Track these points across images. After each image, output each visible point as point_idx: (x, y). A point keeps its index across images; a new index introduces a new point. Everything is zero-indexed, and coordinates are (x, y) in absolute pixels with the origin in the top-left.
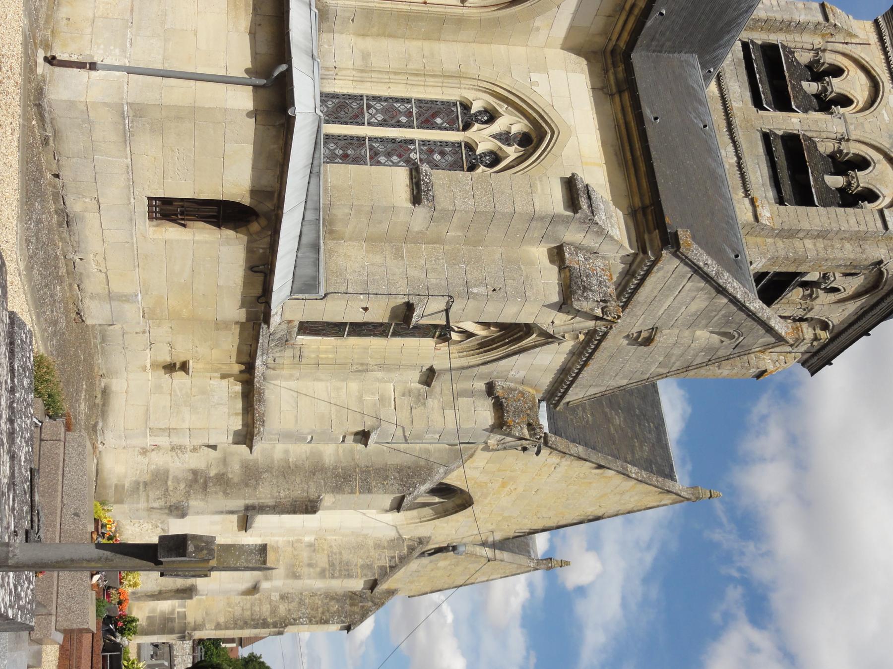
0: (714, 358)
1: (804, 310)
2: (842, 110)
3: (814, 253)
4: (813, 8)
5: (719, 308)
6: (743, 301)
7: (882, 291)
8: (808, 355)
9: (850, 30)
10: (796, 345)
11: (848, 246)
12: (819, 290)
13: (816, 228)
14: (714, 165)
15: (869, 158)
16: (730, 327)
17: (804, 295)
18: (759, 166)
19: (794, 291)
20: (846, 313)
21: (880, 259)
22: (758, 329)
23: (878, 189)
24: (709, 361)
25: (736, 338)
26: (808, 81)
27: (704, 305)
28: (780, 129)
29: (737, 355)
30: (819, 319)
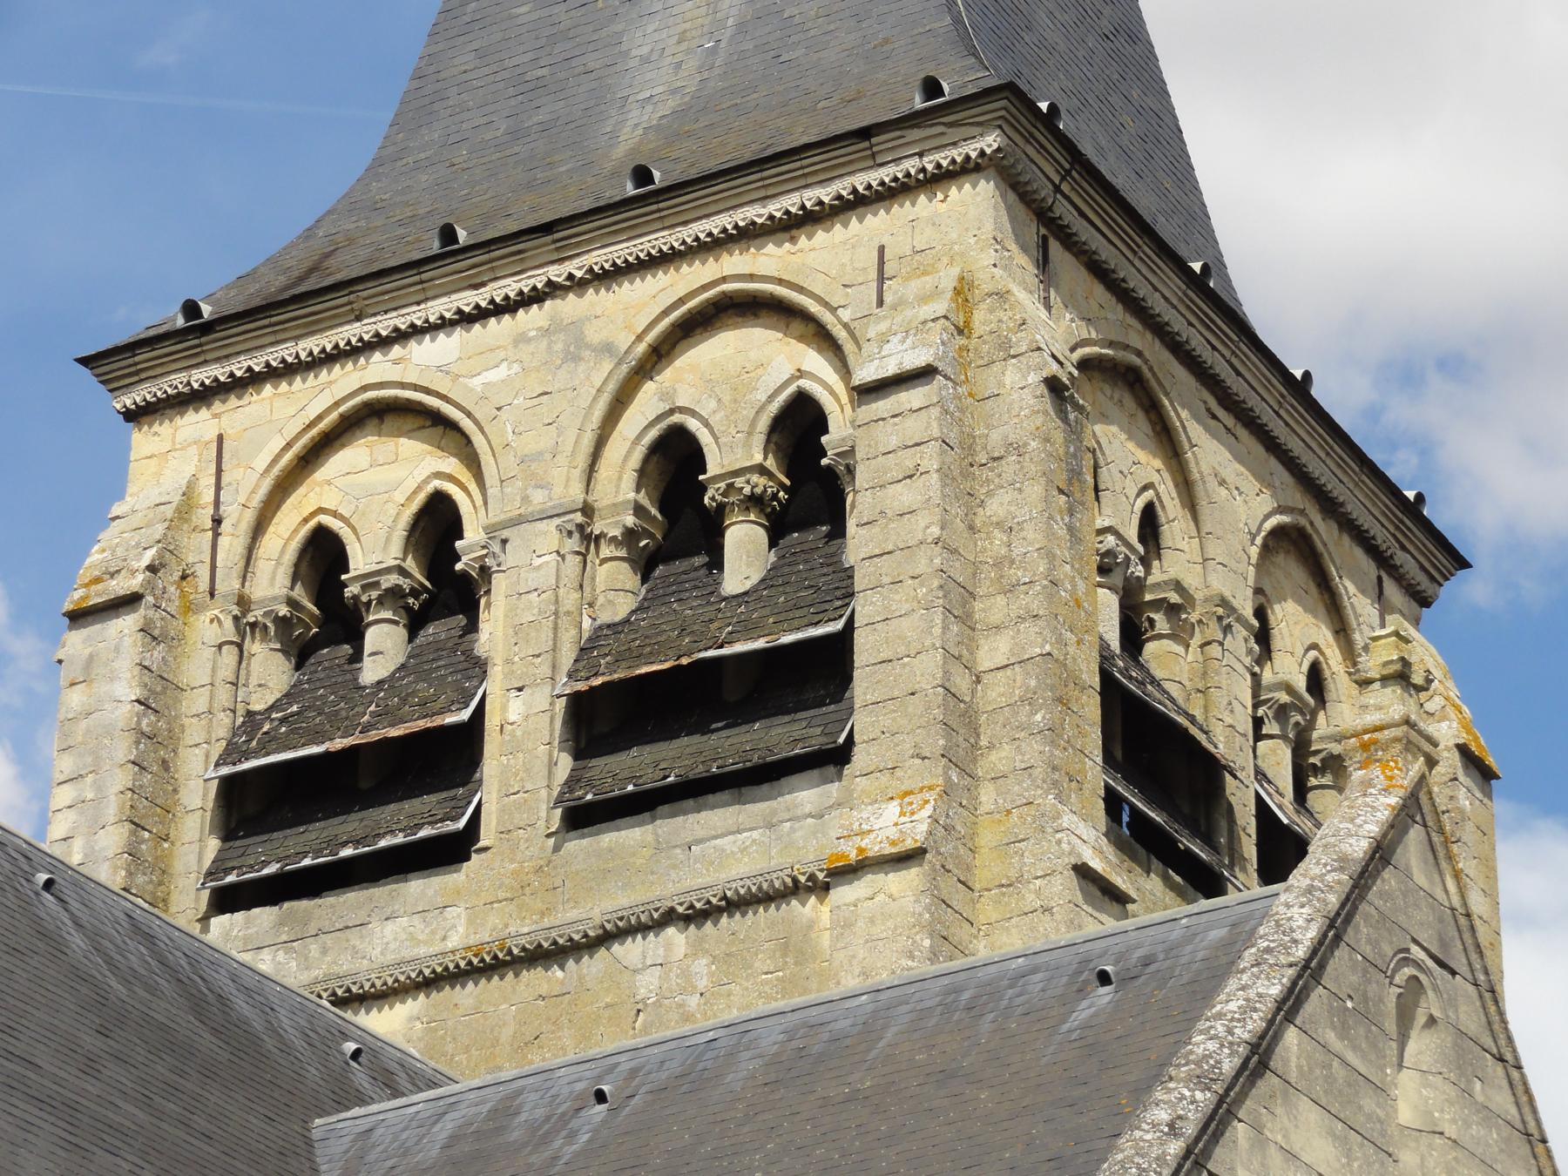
0: (1488, 1042)
1: (1227, 629)
2: (472, 535)
3: (1030, 629)
4: (88, 651)
5: (1319, 1056)
6: (1291, 972)
7: (1147, 354)
8: (1390, 587)
9: (169, 511)
10: (1427, 747)
11: (997, 506)
12: (1150, 580)
13: (937, 631)
14: (748, 1064)
15: (654, 433)
16: (1381, 1000)
17: (1172, 637)
18: (699, 842)
19: (1158, 673)
20: (1233, 470)
21: (1043, 389)
22: (1381, 894)
23: (771, 398)
24: (1501, 1060)
25: (1415, 972)
26: (357, 657)
27: (1310, 1114)
28: (552, 764)
29: (1474, 956)
30: (1258, 567)
